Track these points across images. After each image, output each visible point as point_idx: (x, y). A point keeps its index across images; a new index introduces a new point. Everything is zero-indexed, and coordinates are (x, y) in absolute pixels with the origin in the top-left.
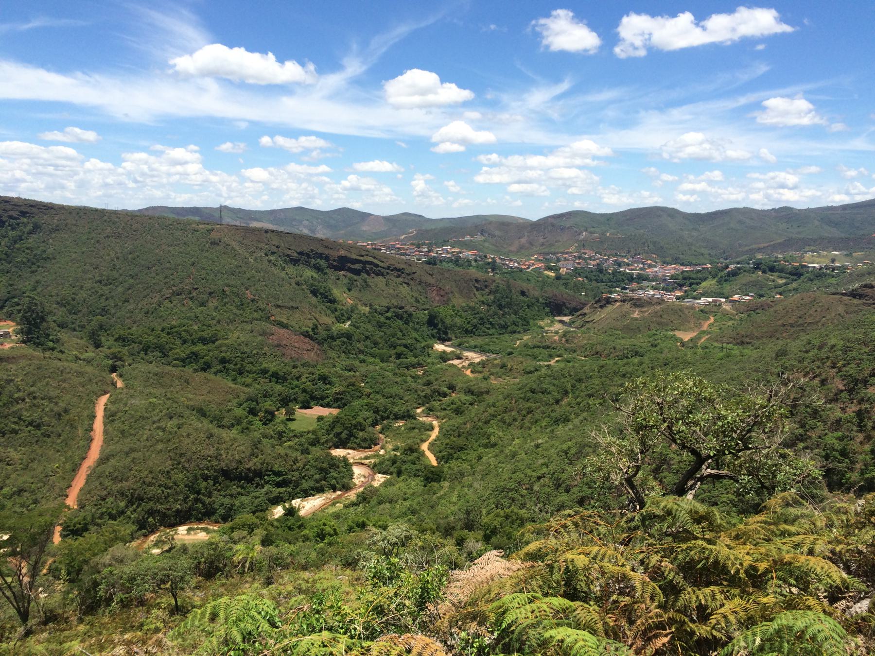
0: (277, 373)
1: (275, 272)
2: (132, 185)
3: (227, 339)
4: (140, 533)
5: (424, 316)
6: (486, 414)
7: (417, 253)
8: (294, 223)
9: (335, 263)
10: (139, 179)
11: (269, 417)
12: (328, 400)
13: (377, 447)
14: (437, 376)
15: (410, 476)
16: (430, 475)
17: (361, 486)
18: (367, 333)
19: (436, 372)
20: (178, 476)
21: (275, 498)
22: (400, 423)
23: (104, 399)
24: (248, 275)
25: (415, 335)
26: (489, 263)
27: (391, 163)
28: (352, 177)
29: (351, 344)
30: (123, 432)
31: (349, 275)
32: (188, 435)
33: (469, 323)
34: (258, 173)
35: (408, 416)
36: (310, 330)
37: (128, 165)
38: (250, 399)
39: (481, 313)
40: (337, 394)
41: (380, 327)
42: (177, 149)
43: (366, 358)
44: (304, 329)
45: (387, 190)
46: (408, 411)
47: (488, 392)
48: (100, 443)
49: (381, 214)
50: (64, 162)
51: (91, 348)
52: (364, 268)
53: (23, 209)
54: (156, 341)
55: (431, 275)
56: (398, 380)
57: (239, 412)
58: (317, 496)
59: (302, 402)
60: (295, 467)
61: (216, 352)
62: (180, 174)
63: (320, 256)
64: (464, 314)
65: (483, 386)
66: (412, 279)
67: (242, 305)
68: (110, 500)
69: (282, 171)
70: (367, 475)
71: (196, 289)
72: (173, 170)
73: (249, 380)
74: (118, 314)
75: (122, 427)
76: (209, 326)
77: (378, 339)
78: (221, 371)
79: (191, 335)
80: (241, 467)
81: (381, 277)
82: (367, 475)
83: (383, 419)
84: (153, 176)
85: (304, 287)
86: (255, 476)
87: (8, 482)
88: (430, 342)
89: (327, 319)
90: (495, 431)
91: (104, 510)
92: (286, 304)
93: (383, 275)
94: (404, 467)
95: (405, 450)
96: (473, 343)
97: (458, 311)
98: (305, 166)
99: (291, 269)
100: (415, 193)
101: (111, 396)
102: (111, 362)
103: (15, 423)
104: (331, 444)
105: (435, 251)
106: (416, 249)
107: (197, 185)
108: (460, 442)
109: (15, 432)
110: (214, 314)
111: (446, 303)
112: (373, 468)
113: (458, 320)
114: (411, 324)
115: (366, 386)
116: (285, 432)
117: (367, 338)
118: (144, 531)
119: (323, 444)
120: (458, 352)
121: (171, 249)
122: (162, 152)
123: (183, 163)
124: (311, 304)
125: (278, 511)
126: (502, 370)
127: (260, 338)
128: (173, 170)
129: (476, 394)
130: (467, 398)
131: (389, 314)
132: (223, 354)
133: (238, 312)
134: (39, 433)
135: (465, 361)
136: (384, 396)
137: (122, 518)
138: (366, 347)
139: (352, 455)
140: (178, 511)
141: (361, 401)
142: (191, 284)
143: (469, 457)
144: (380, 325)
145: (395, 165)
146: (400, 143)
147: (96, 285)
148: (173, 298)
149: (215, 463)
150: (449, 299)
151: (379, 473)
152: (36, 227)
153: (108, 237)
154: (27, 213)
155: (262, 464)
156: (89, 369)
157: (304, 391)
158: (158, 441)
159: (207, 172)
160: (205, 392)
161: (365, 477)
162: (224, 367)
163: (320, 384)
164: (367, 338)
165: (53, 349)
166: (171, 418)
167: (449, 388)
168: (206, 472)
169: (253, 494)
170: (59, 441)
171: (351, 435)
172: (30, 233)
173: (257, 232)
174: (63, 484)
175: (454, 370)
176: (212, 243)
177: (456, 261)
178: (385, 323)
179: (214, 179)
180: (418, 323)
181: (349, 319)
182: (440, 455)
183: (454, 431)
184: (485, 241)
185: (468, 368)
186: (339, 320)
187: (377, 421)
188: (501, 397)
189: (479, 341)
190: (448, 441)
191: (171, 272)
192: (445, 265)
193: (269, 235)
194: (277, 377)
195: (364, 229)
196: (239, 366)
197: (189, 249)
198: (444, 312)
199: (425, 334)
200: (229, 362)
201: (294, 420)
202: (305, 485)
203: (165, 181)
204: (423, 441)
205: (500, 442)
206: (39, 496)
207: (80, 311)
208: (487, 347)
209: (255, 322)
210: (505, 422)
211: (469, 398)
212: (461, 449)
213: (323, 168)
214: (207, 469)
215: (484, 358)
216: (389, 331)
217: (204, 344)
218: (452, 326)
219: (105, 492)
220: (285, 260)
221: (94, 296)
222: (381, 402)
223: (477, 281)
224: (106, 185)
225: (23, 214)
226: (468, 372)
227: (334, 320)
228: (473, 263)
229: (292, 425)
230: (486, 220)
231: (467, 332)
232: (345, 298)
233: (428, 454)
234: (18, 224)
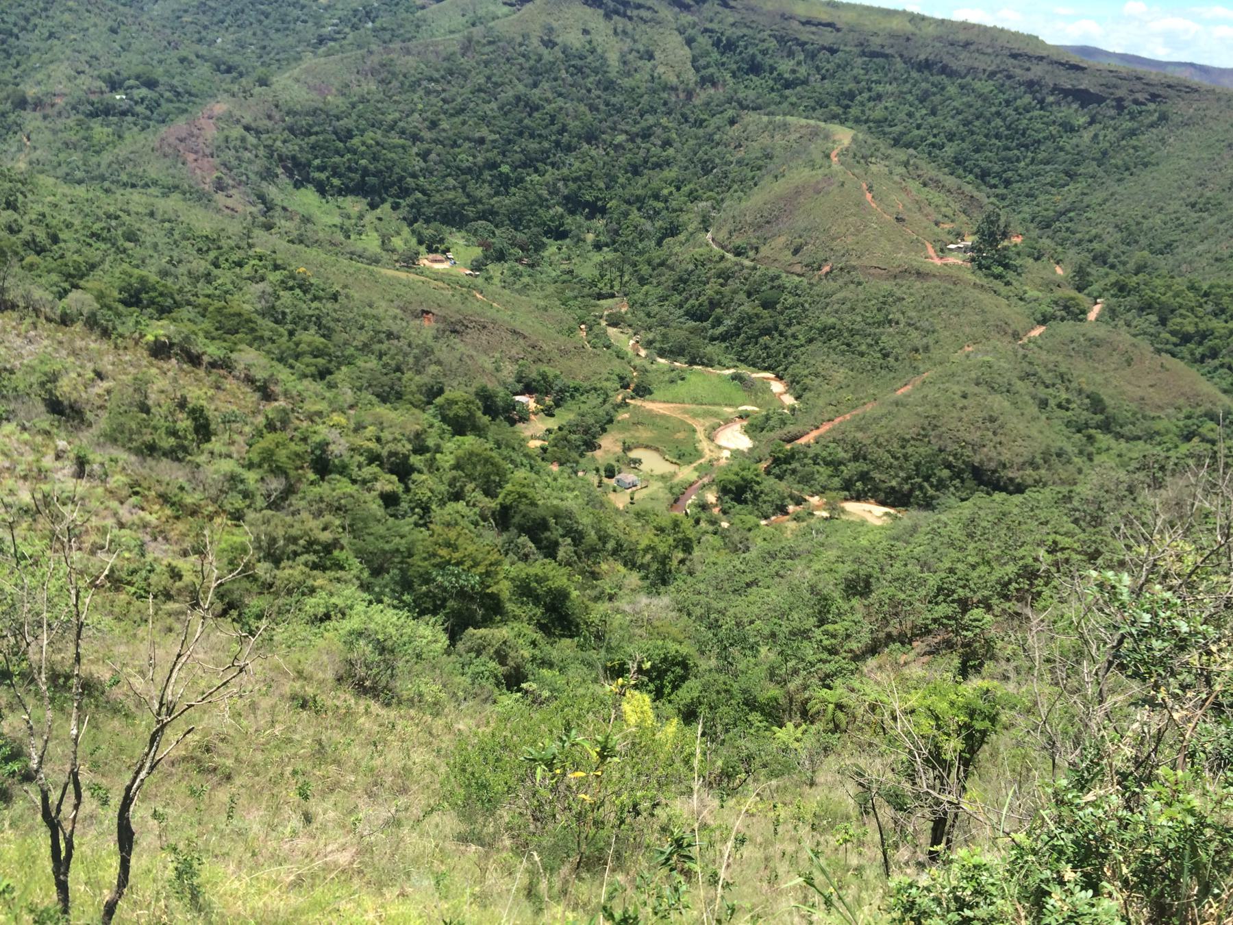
140: (892, 488)
149: (968, 452)
152: (1163, 117)
154: (1159, 96)
168: (951, 458)
172: (1152, 125)
214: (955, 455)
225: (1154, 97)
234: (1140, 113)
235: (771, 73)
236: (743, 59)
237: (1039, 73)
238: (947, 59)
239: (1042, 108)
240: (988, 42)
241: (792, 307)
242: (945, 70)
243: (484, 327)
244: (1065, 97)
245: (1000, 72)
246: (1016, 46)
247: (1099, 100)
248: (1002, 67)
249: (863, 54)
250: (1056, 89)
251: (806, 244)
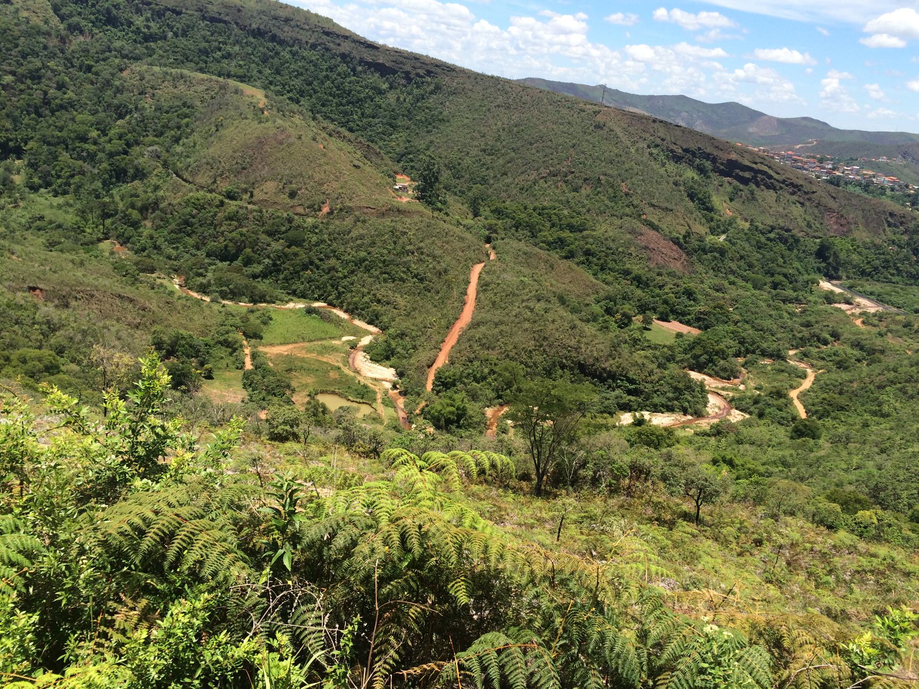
0: (640, 278)
1: (655, 167)
2: (513, 51)
3: (594, 230)
4: (496, 401)
5: (813, 245)
6: (881, 377)
7: (818, 169)
8: (671, 113)
9: (722, 167)
10: (521, 46)
11: (626, 321)
12: (689, 317)
13: (736, 381)
14: (819, 319)
15: (773, 422)
16: (801, 427)
17: (714, 417)
18: (742, 253)
19: (818, 313)
20: (538, 358)
21: (624, 404)
22: (767, 361)
23: (478, 268)
24: (627, 166)
25: (797, 264)
26: (909, 195)
27: (802, 52)
28: (750, 66)
29: (723, 261)
30: (494, 303)
31: (736, 183)
32: (553, 321)
33: (868, 263)
34: (642, 51)
35: (778, 356)
36: (681, 237)
37: (514, 30)
38: (609, 298)
39: (889, 254)
40: (701, 313)
41: (759, 248)
42: (565, 17)
43: (736, 280)
44: (675, 234)
45: (788, 86)
46: (779, 350)
47: (882, 352)
48: (472, 308)
49: (776, 116)
50: (456, 22)
51: (471, 216)
52: (755, 177)
53: (428, 68)
54: (527, 219)
55: (834, 198)
56: (773, 313)
57: (597, 309)
58: (666, 414)
59: (661, 313)
60: (649, 379)
61: (582, 243)
62: (562, 44)
63: (707, 156)
64: (865, 251)
65: (878, 343)
66: (809, 199)
67: (615, 197)
68: (476, 363)
69: (670, 51)
70: (722, 407)
71: (572, 173)
72: (556, 39)
73: (610, 278)
74: (496, 186)
75: (494, 298)
76: (579, 213)
77: (755, 262)
78: (583, 263)
79: (560, 220)
80: (597, 364)
81: (772, 191)
82: (722, 407)
83: (748, 351)
84: (535, 44)
85: (682, 188)
86: (609, 377)
87: (393, 323)
88: (813, 276)
89: (701, 229)
90: (890, 400)
91: (471, 371)
92: (661, 204)
93: (775, 189)
94: (767, 411)
95: (771, 393)
96: (868, 288)
97: (858, 247)
98: (697, 48)
99: (671, 167)
100: (823, 94)
101: (485, 266)
102: (487, 233)
103: (404, 272)
104: (686, 364)
105: (841, 170)
106: (817, 164)
107: (576, 58)
108: (842, 400)
109: (402, 280)
110: (585, 201)
111: (845, 234)
112: (731, 401)
113: (855, 257)
114: (795, 251)
115: (736, 312)
116: (640, 340)
117: (742, 257)
118: (501, 400)
119: (677, 362)
120: (849, 296)
121: (555, 127)
122: (550, 19)
123: (567, 32)
124: (687, 208)
125: (627, 418)
126: (906, 330)
127: (629, 236)
128: (556, 39)
129: (870, 353)
130: (855, 352)
131: (772, 235)
132: (589, 246)
133: (610, 204)
134: (422, 286)
135: (855, 308)
136: (753, 327)
137: (484, 383)
138: (739, 267)
139: (711, 383)
141: (726, 327)
142: (569, 166)
143: (850, 421)
144: (759, 246)
145: (807, 57)
146: (820, 29)
147: (480, 154)
148: (549, 178)
150: (850, 231)
151: (737, 409)
152: (438, 88)
153: (499, 106)
154: (432, 72)
155: (618, 367)
156: (468, 235)
157: (665, 302)
158: (525, 320)
159: (590, 45)
160: (567, 281)
161: (720, 408)
162: (587, 260)
163: (684, 298)
164: (742, 257)
165: (440, 210)
166: (539, 300)
167: (832, 336)
169: (604, 394)
170: (437, 298)
171: (711, 361)
172: (432, 93)
173: (644, 121)
174: (436, 338)
175: (841, 316)
176: (595, 127)
177: (867, 186)
178: (766, 245)
179: (595, 53)
180: (804, 251)
181: (724, 232)
182: (813, 409)
183: (835, 386)
184: (905, 166)
185: (859, 317)
186: (713, 231)
187: (740, 352)
188: (906, 362)
189: (877, 287)
190: (825, 395)
191: (551, 151)
192: (850, 188)
193: (656, 125)
194: (638, 281)
195: (751, 130)
196: (602, 261)
197: (572, 130)
198: (841, 245)
199: (810, 267)
200: (593, 255)
201: (649, 330)
202: (656, 400)
203: (545, 50)
204: (792, 387)
205: (894, 414)
206: (418, 343)
207: (463, 177)
208: (887, 298)
209: (626, 218)
210: (905, 393)
211: (857, 353)
212: (842, 408)
213: (719, 52)
214: (566, 358)
215: (880, 309)
216: (768, 255)
217: (571, 232)
218: (846, 262)
219: (473, 356)
220: (667, 156)
221: (477, 164)
222: (749, 332)
223: (891, 215)
224: (490, 50)
225: (429, 73)
226: (858, 322)
227: (708, 230)
228: (888, 192)
229: (647, 334)
230: (911, 140)
231: (863, 273)
232: (724, 208)
233: (797, 403)
234: (423, 83)
235: (130, 27)
236: (99, 11)
237: (348, 48)
238: (275, 31)
239: (354, 75)
240: (304, 21)
241: (317, 244)
242: (274, 38)
243: (92, 296)
244: (369, 68)
245: (319, 45)
246: (326, 26)
247: (394, 72)
248: (320, 41)
249: (204, 18)
250: (362, 62)
251: (300, 189)
